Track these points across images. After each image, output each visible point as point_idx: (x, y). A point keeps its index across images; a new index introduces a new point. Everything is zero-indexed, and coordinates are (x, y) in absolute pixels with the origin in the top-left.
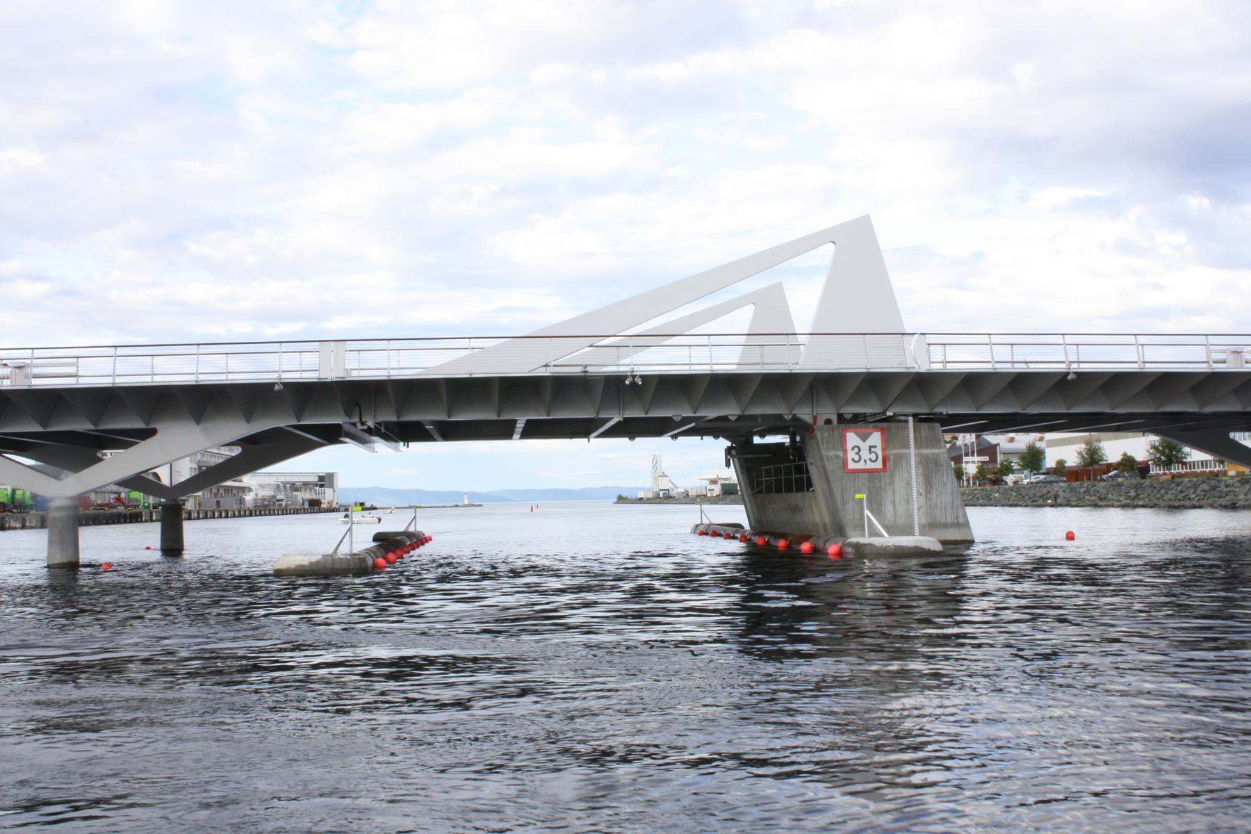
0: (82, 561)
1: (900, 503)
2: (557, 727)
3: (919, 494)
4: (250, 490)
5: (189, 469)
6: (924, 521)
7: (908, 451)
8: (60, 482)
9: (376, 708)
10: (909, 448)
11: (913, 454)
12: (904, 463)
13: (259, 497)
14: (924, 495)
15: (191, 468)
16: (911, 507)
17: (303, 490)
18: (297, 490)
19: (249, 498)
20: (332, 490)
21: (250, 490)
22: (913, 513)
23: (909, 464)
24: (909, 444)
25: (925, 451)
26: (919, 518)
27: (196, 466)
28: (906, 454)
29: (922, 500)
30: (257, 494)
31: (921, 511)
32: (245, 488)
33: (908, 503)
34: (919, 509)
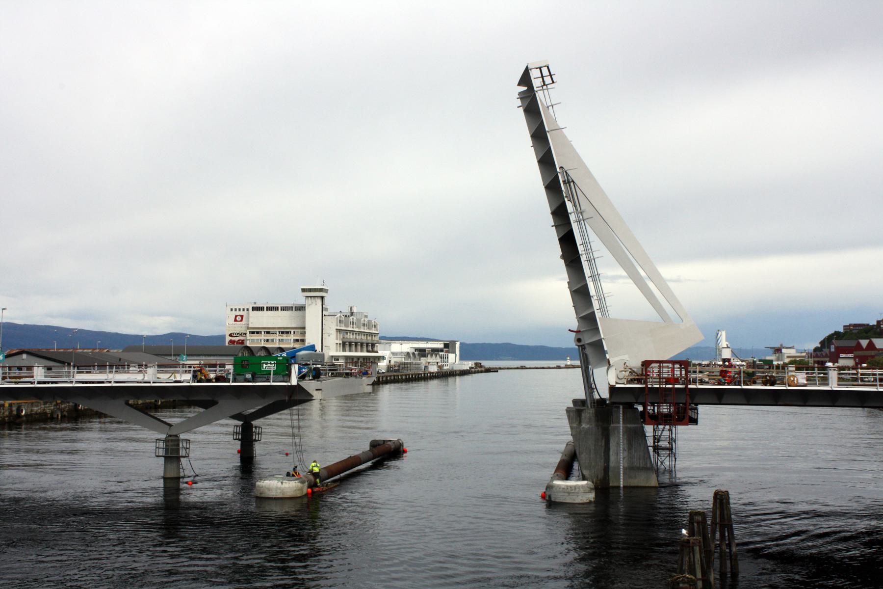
0: (163, 459)
1: (613, 454)
2: (147, 568)
3: (624, 450)
4: (383, 358)
5: (335, 345)
6: (626, 465)
7: (618, 425)
8: (218, 404)
9: (65, 470)
10: (619, 423)
11: (621, 427)
12: (616, 432)
13: (392, 363)
14: (627, 451)
15: (337, 344)
16: (619, 457)
17: (429, 356)
18: (425, 356)
19: (382, 365)
20: (454, 355)
21: (383, 358)
22: (620, 461)
23: (619, 433)
24: (619, 420)
25: (629, 426)
26: (623, 464)
27: (341, 342)
28: (618, 427)
29: (626, 453)
30: (390, 361)
31: (625, 461)
32: (380, 357)
33: (618, 455)
34: (624, 458)
